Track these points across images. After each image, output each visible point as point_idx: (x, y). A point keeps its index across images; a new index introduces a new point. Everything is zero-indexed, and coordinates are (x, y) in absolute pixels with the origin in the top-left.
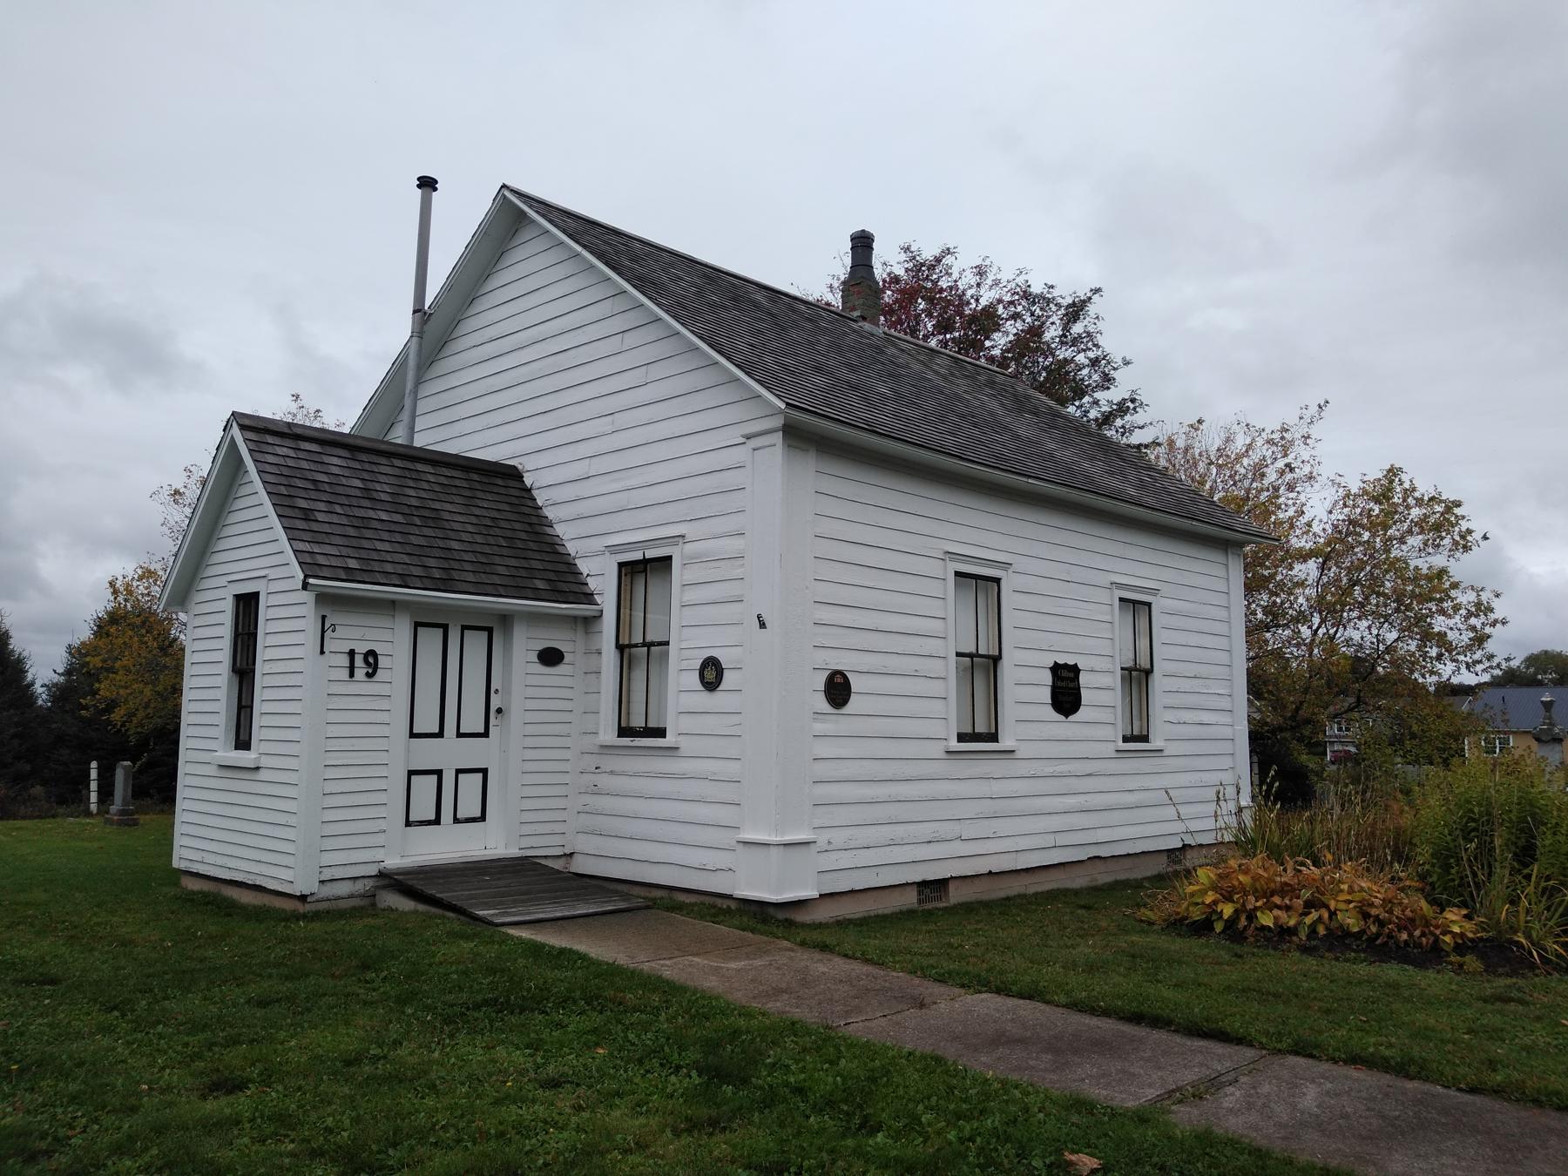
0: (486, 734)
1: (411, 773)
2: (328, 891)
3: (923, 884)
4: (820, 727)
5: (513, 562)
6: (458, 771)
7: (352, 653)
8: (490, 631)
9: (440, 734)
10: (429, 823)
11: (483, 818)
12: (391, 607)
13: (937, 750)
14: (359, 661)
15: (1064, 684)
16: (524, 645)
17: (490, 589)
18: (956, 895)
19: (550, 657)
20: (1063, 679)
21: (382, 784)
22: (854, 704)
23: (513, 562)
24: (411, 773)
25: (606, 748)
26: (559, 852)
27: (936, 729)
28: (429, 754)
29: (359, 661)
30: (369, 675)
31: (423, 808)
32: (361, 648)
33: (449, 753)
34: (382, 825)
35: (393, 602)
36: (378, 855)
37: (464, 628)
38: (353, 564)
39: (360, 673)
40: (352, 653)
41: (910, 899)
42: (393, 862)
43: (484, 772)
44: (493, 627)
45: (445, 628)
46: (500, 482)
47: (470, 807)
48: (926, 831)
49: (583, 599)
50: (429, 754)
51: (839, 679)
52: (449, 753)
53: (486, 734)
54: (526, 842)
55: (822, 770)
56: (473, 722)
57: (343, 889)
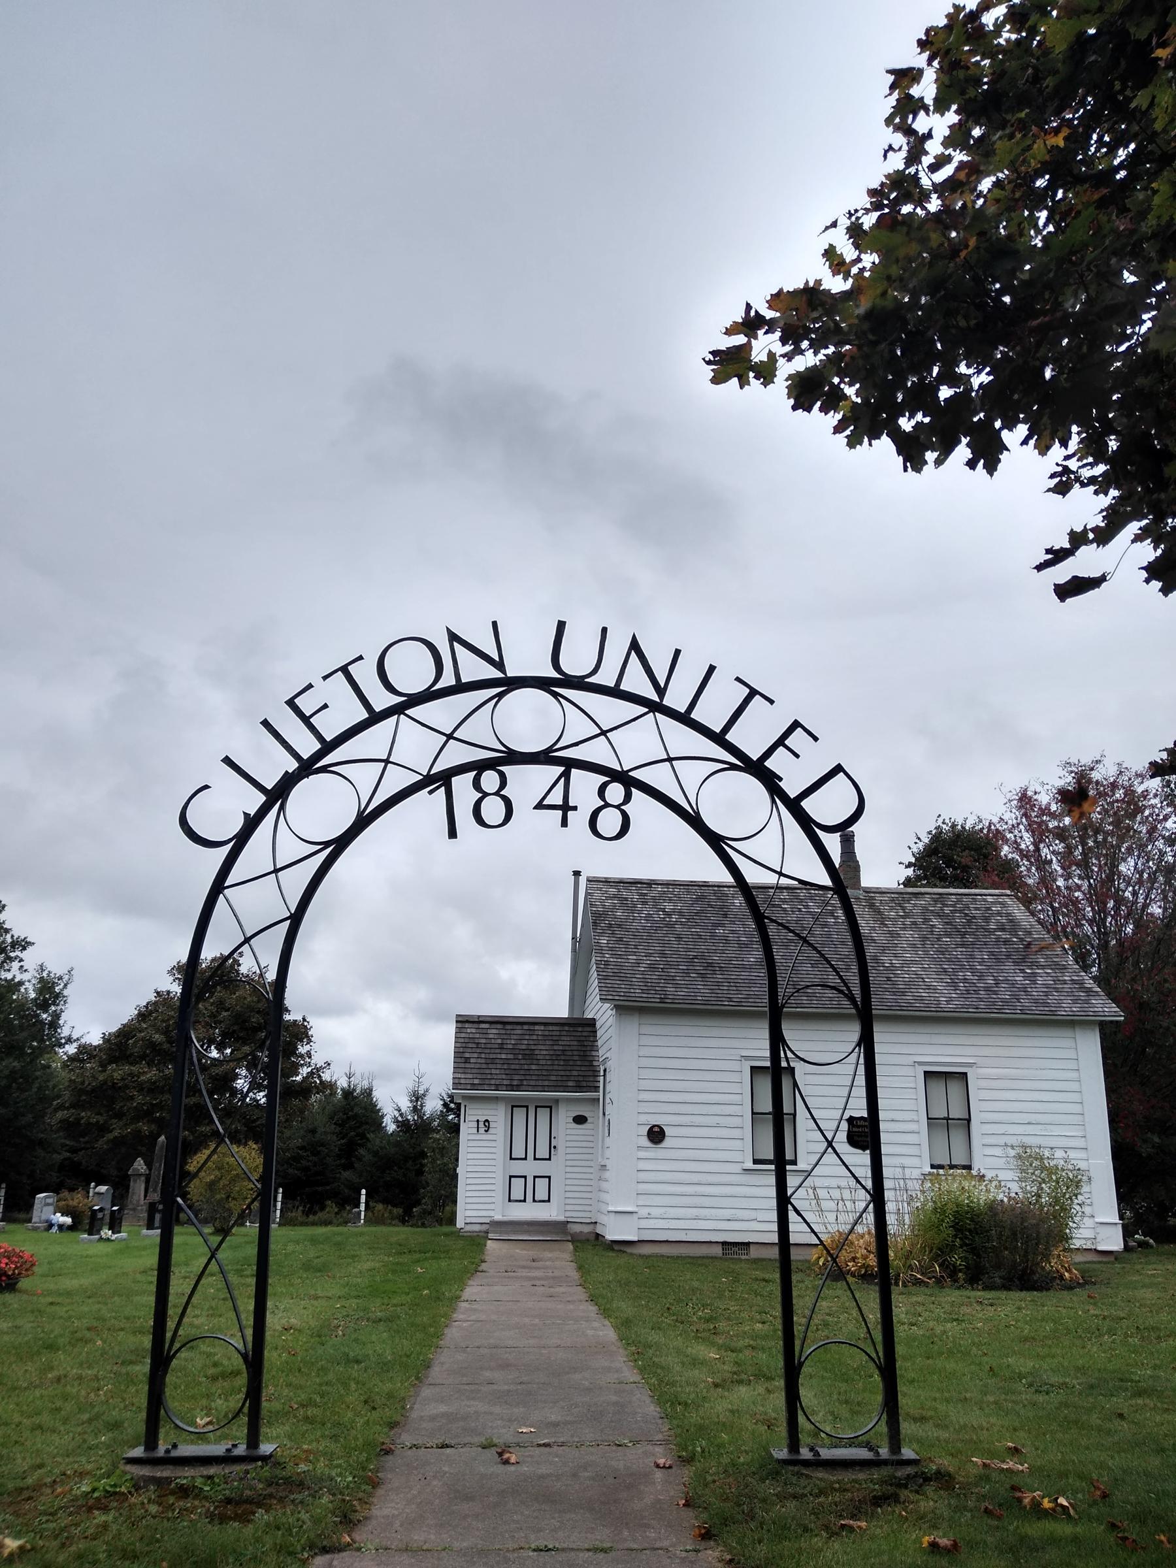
0: (550, 1159)
1: (511, 1177)
2: (468, 1228)
3: (724, 1244)
4: (642, 1154)
5: (563, 1073)
6: (535, 1177)
7: (478, 1121)
8: (551, 1107)
9: (525, 1159)
10: (520, 1201)
11: (549, 1201)
12: (496, 1099)
13: (737, 1168)
14: (481, 1124)
15: (856, 1130)
16: (564, 1117)
17: (540, 1089)
18: (754, 1253)
19: (580, 1120)
20: (854, 1126)
21: (493, 1181)
22: (667, 1142)
23: (563, 1073)
24: (511, 1177)
25: (747, 1171)
26: (588, 1221)
27: (737, 1156)
28: (518, 1168)
29: (481, 1124)
30: (486, 1131)
31: (517, 1193)
32: (482, 1119)
33: (530, 1168)
34: (493, 1200)
35: (497, 1098)
36: (491, 1213)
37: (536, 1107)
38: (476, 1081)
39: (482, 1130)
40: (478, 1121)
41: (718, 1251)
42: (498, 1217)
43: (549, 1177)
44: (550, 1107)
45: (527, 1107)
46: (580, 1029)
47: (541, 1194)
48: (727, 1213)
49: (593, 1089)
50: (518, 1168)
51: (656, 1129)
52: (530, 1168)
53: (550, 1159)
54: (568, 1214)
55: (642, 1176)
56: (543, 1152)
57: (477, 1228)
